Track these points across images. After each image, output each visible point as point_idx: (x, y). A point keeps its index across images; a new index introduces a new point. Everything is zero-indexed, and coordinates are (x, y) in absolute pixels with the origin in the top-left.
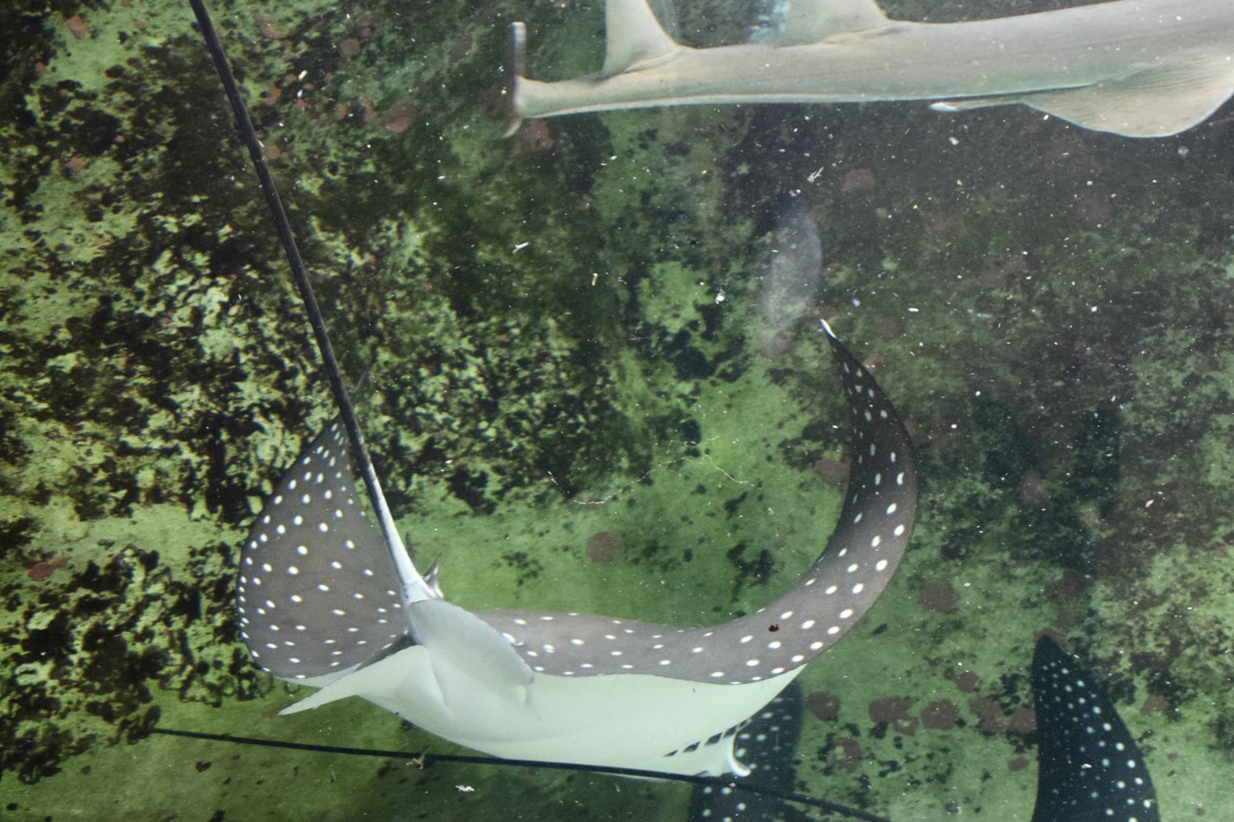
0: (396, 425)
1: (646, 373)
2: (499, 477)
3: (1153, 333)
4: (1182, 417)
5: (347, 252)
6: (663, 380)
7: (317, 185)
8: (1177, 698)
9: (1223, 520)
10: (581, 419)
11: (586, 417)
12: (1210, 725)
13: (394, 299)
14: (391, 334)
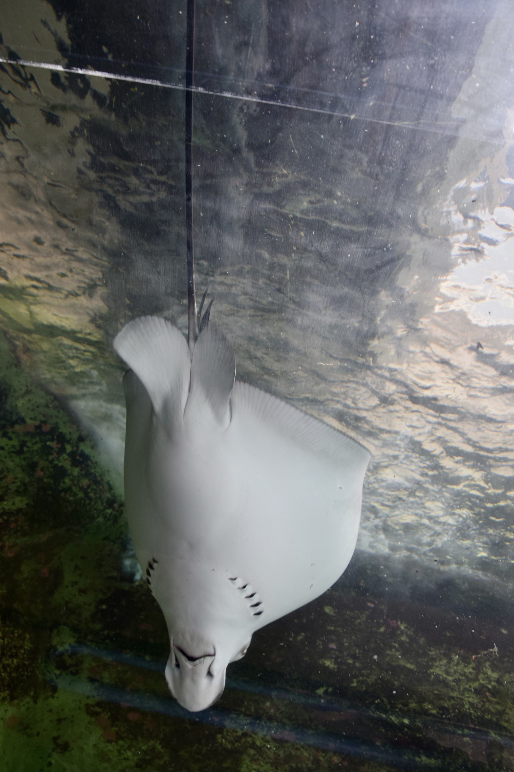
4: (238, 745)
10: (26, 673)
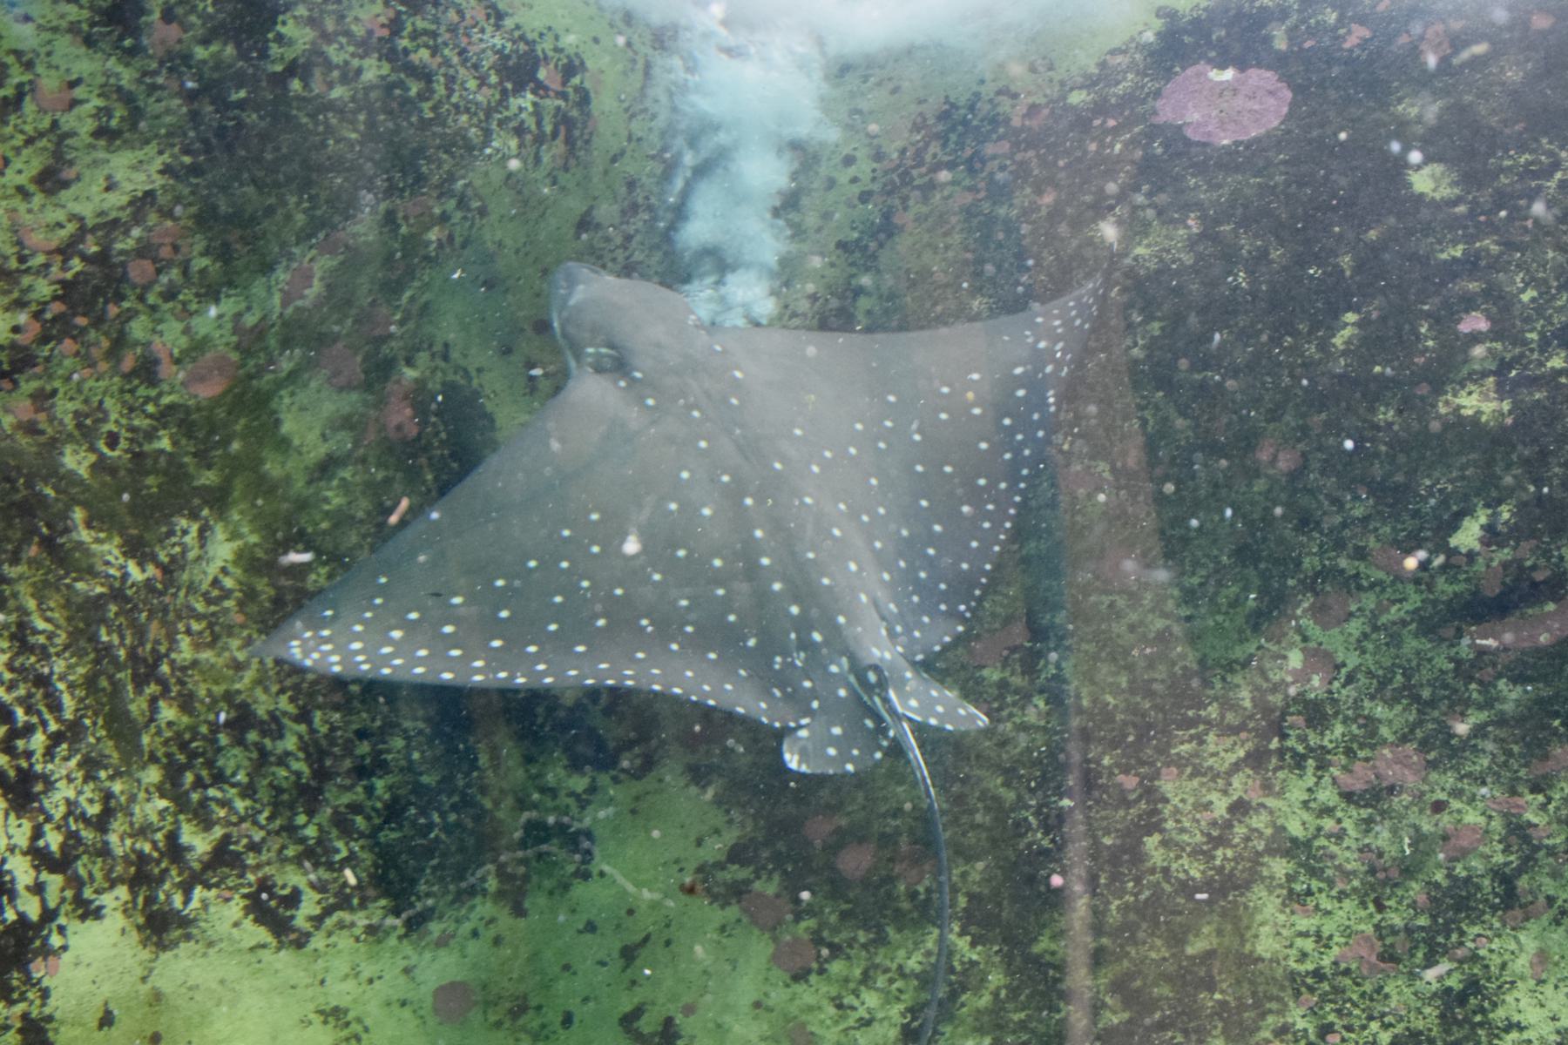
1: (529, 760)
2: (318, 897)
3: (1192, 738)
4: (1225, 858)
5: (121, 561)
7: (86, 464)
9: (1274, 1006)
11: (443, 815)
13: (188, 632)
14: (181, 683)
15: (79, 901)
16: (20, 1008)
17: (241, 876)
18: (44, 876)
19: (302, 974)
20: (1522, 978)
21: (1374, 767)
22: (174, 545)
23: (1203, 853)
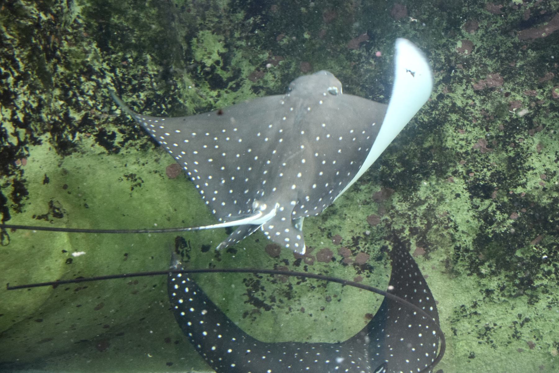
0: (67, 106)
2: (122, 135)
5: (37, 12)
6: (203, 89)
8: (429, 249)
9: (452, 164)
10: (164, 107)
11: (166, 106)
12: (442, 262)
14: (64, 58)
15: (32, 138)
16: (12, 177)
17: (93, 128)
18: (18, 129)
19: (118, 163)
20: (534, 152)
21: (486, 81)
22: (58, 6)
23: (428, 112)
